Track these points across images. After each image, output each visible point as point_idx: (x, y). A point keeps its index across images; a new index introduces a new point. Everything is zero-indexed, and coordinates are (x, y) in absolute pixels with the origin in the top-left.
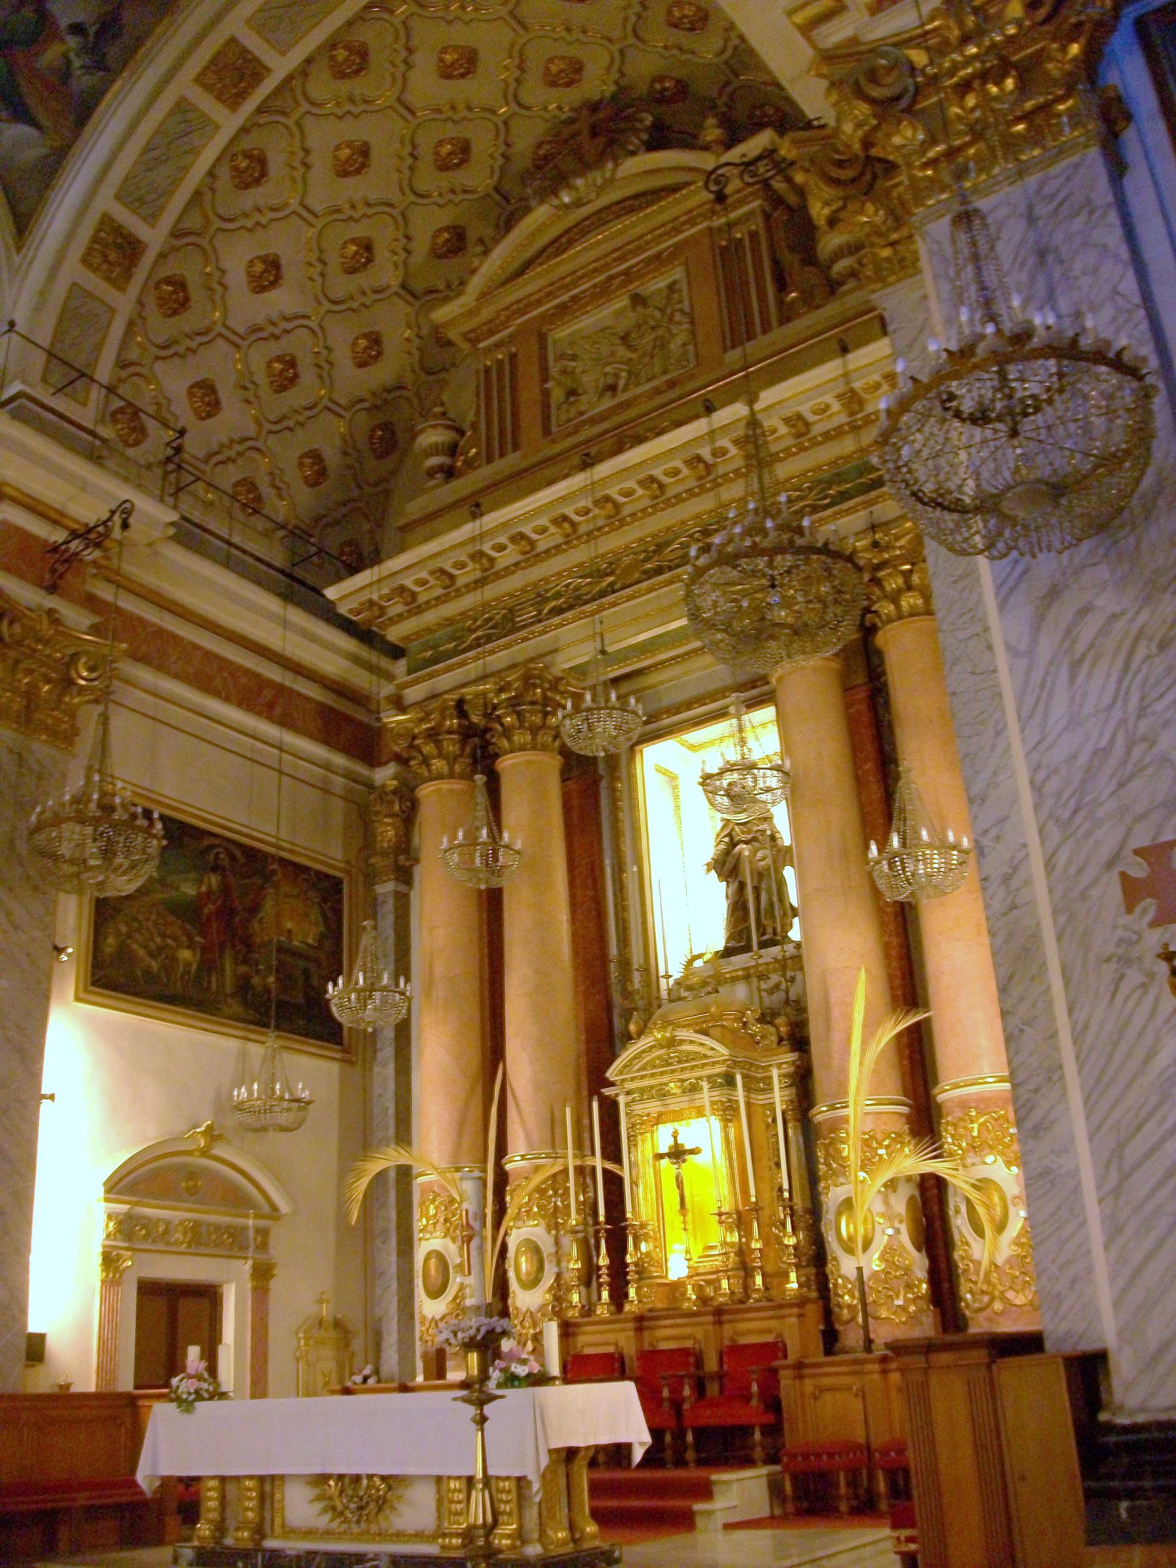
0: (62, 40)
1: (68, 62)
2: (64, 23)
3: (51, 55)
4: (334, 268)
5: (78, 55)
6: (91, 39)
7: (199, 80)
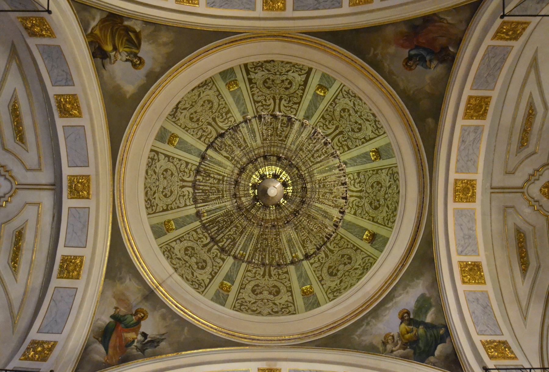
0: (137, 335)
1: (133, 342)
2: (142, 330)
3: (130, 336)
5: (137, 342)
6: (146, 341)
7: (464, 118)
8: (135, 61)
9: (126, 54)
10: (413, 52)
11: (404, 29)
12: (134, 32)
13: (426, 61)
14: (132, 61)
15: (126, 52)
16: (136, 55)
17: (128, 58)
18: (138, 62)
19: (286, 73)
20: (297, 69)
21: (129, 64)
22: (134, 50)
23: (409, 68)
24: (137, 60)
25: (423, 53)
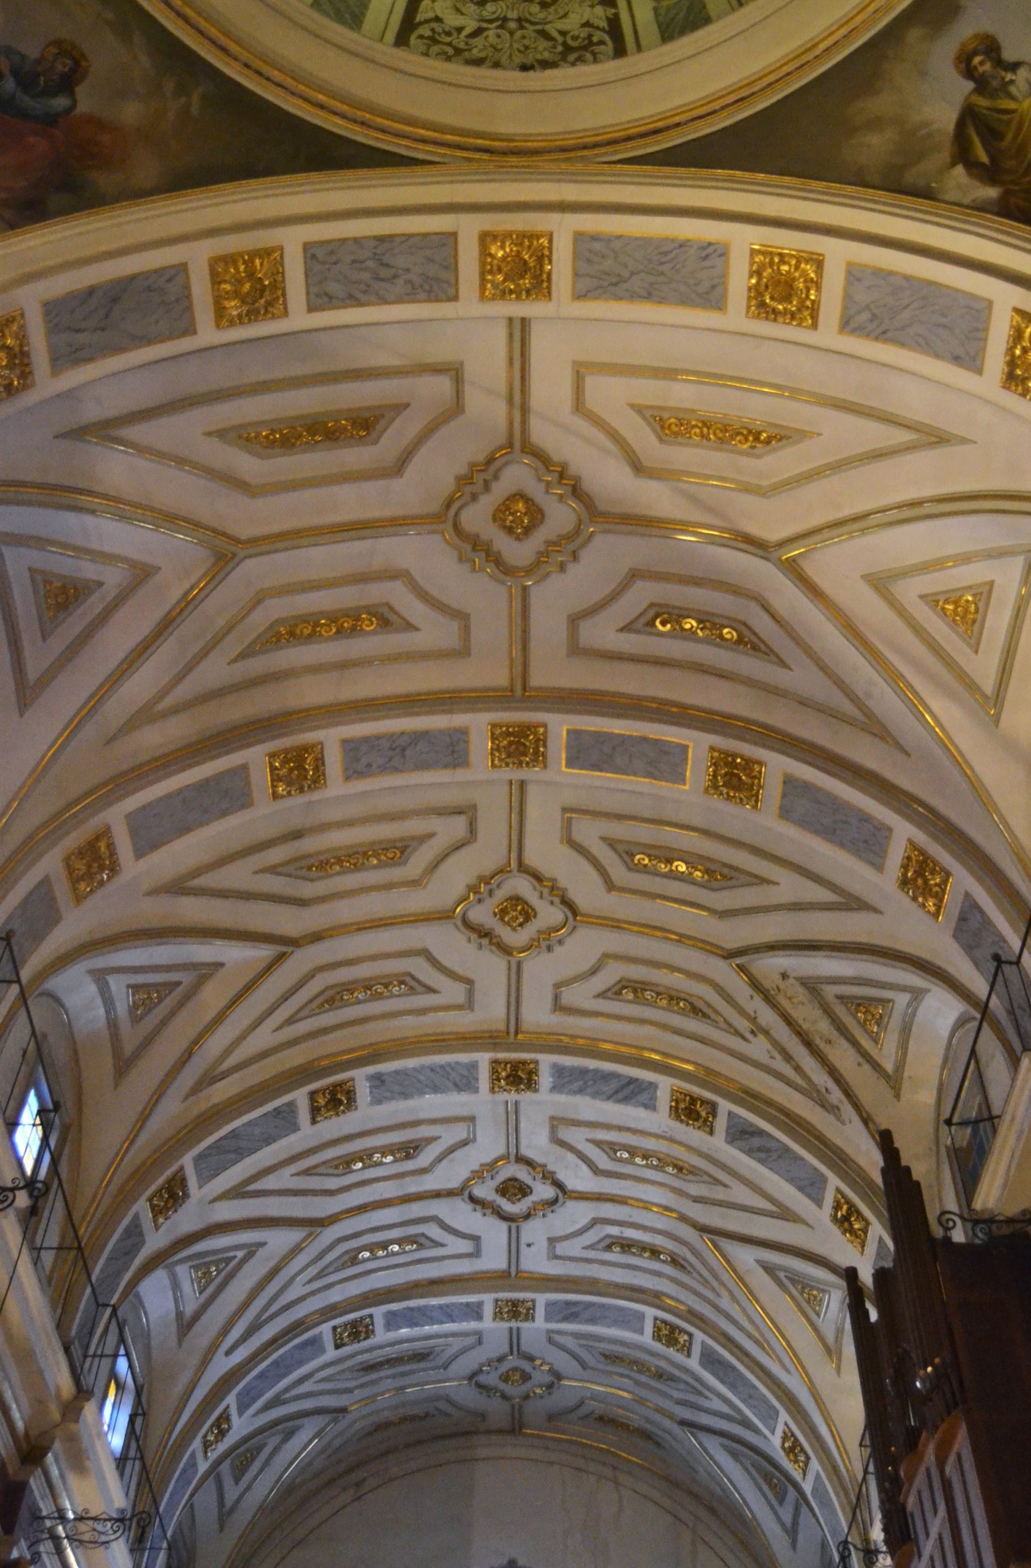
4: (503, 543)
8: (987, 67)
9: (1013, 89)
10: (61, 102)
11: (103, 180)
12: (972, 166)
13: (11, 71)
14: (999, 63)
15: (1013, 98)
16: (982, 85)
17: (1009, 76)
18: (977, 60)
19: (485, 25)
20: (448, 39)
21: (1009, 55)
22: (982, 102)
23: (65, 49)
24: (981, 69)
25: (26, 101)
